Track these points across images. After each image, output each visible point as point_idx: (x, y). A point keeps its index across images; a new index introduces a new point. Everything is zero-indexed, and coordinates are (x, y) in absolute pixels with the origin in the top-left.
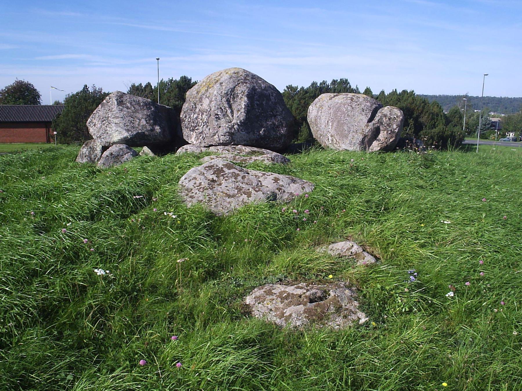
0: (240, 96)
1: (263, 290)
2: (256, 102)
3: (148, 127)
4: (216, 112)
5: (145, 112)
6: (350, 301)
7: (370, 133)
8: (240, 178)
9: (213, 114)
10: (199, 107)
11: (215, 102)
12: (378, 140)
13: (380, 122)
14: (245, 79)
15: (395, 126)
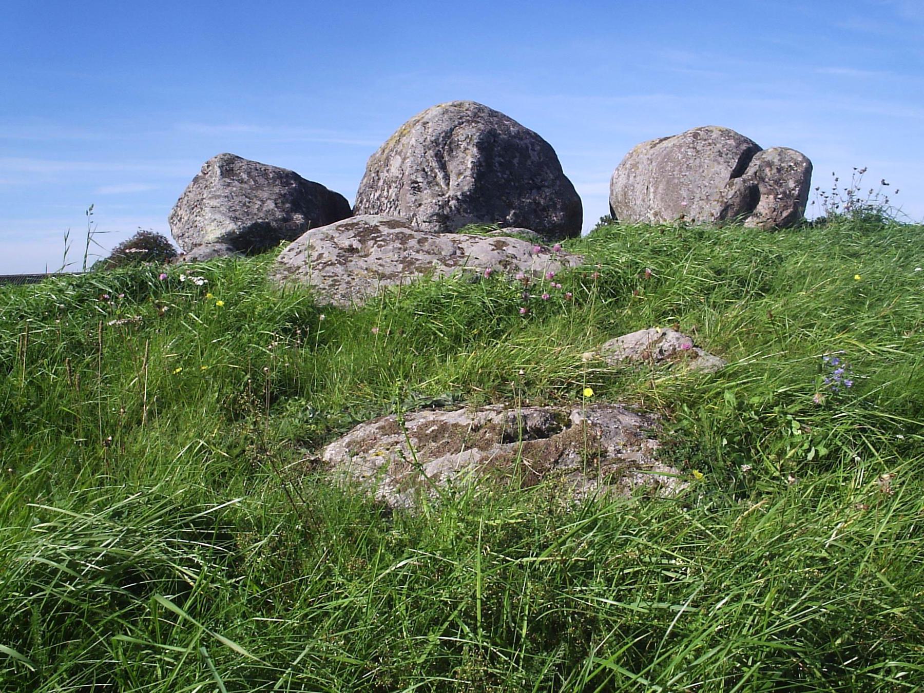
0: (463, 145)
1: (377, 425)
2: (497, 159)
3: (278, 213)
4: (413, 177)
5: (277, 189)
6: (634, 437)
7: (738, 200)
8: (412, 243)
9: (406, 181)
10: (384, 175)
11: (412, 159)
12: (756, 215)
13: (759, 176)
14: (475, 115)
15: (791, 184)
